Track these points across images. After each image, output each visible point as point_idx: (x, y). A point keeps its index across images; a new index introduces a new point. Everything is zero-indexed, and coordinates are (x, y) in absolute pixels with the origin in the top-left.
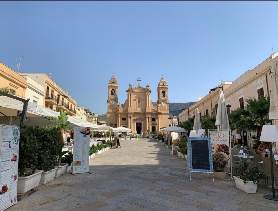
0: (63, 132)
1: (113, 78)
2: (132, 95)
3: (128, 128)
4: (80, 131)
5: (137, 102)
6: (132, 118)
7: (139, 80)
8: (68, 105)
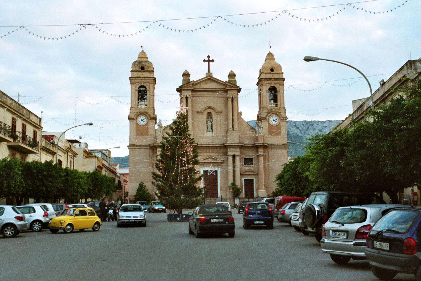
1: (143, 55)
4: (143, 182)
7: (209, 61)
8: (14, 126)
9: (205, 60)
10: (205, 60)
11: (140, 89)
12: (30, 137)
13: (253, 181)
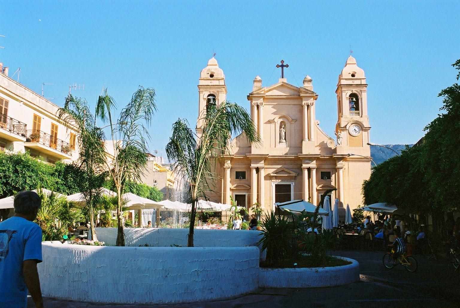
0: (365, 224)
2: (261, 108)
3: (221, 203)
5: (278, 126)
6: (263, 173)
7: (282, 66)
9: (278, 65)
10: (278, 65)
11: (209, 97)
12: (62, 141)
13: (291, 186)
